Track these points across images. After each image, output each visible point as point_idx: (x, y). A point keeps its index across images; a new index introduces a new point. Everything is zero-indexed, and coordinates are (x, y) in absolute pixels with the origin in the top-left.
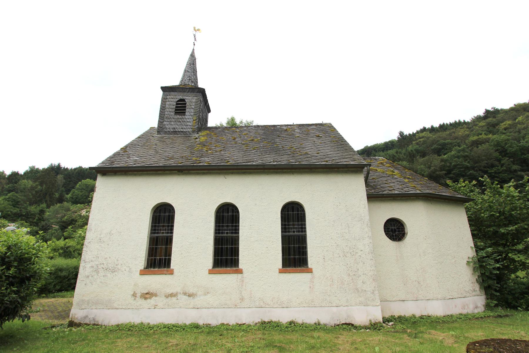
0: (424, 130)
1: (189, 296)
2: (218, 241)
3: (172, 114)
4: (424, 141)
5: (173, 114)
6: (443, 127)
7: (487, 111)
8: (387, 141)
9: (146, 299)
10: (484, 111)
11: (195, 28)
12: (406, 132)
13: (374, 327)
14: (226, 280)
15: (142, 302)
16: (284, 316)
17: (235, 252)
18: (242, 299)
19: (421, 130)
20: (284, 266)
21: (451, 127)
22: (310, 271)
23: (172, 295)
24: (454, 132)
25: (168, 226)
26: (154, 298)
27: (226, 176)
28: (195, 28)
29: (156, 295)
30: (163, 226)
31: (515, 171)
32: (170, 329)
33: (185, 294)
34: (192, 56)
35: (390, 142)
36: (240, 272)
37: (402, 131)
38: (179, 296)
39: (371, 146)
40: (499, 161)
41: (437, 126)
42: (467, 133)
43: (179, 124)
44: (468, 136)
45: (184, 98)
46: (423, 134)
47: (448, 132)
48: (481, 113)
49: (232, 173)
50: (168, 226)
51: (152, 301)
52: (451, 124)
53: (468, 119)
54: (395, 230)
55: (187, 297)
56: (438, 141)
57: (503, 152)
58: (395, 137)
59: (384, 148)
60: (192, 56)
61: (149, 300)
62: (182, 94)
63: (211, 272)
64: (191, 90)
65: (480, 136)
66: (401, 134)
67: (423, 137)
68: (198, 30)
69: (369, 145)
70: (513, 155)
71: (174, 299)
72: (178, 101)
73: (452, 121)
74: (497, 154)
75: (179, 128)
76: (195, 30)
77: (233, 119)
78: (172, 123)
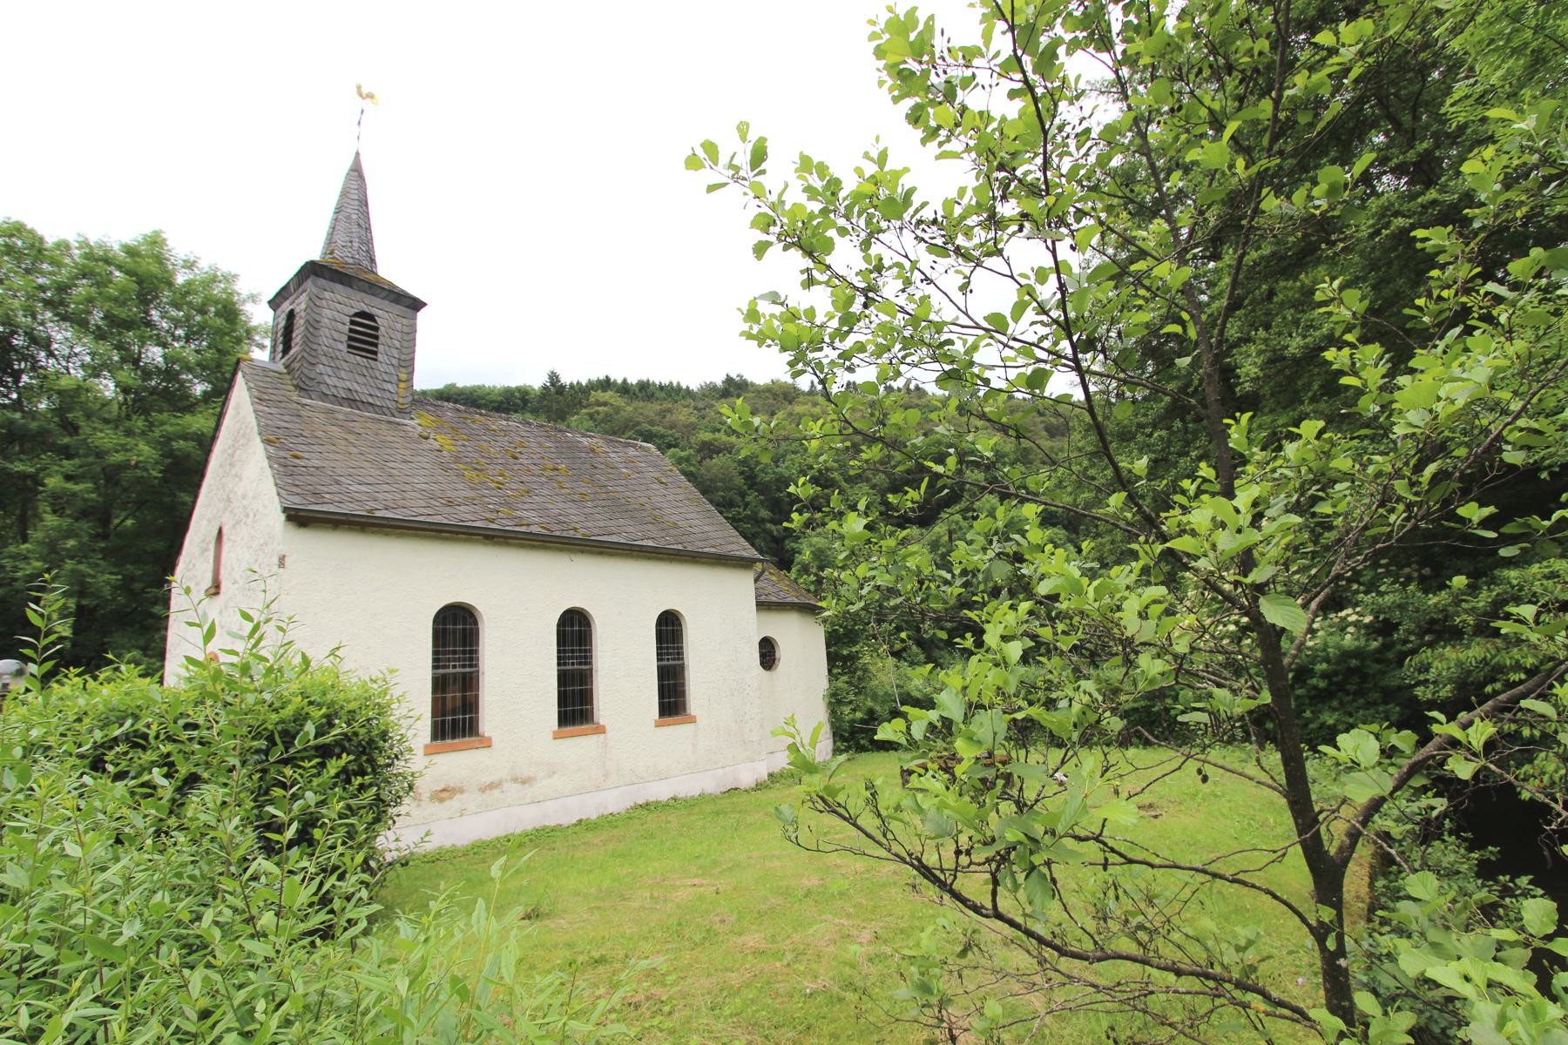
0: (606, 384)
1: (523, 782)
2: (563, 678)
3: (341, 346)
4: (607, 415)
5: (344, 347)
6: (645, 390)
7: (729, 380)
8: (513, 385)
9: (441, 800)
10: (724, 377)
11: (359, 88)
12: (566, 379)
13: (759, 787)
14: (580, 746)
15: (436, 807)
16: (661, 791)
17: (470, 706)
18: (606, 775)
19: (599, 380)
20: (435, 737)
21: (663, 394)
22: (693, 720)
23: (492, 786)
24: (669, 411)
25: (464, 652)
26: (458, 796)
27: (573, 557)
28: (359, 88)
29: (461, 791)
30: (454, 652)
31: (763, 521)
32: (482, 851)
33: (515, 780)
34: (356, 171)
35: (518, 389)
36: (601, 730)
37: (558, 371)
38: (506, 785)
39: (465, 388)
40: (743, 495)
41: (635, 382)
42: (693, 419)
43: (359, 379)
44: (693, 427)
45: (374, 311)
46: (608, 396)
47: (657, 407)
48: (719, 380)
49: (582, 552)
50: (464, 652)
51: (454, 804)
52: (661, 388)
53: (693, 383)
54: (768, 653)
55: (518, 786)
56: (638, 423)
57: (751, 478)
58: (536, 380)
59: (501, 402)
60: (356, 171)
61: (447, 803)
62: (368, 298)
63: (556, 736)
64: (392, 297)
65: (717, 435)
66: (554, 377)
67: (605, 404)
68: (371, 96)
69: (460, 385)
70: (763, 489)
71: (496, 792)
72: (356, 315)
73: (665, 382)
74: (739, 481)
75: (362, 390)
76: (360, 94)
77: (156, 241)
78: (343, 374)
